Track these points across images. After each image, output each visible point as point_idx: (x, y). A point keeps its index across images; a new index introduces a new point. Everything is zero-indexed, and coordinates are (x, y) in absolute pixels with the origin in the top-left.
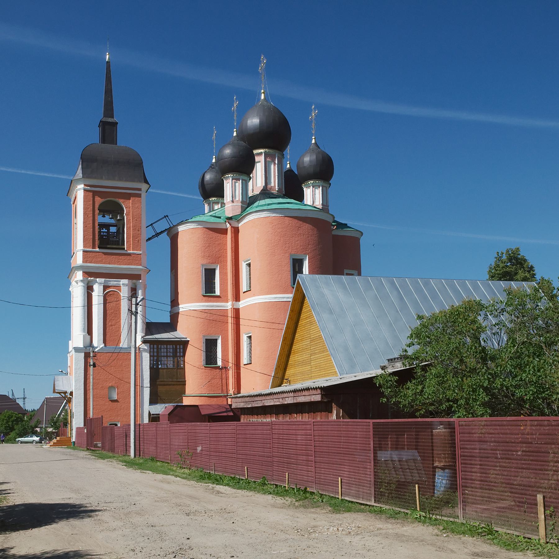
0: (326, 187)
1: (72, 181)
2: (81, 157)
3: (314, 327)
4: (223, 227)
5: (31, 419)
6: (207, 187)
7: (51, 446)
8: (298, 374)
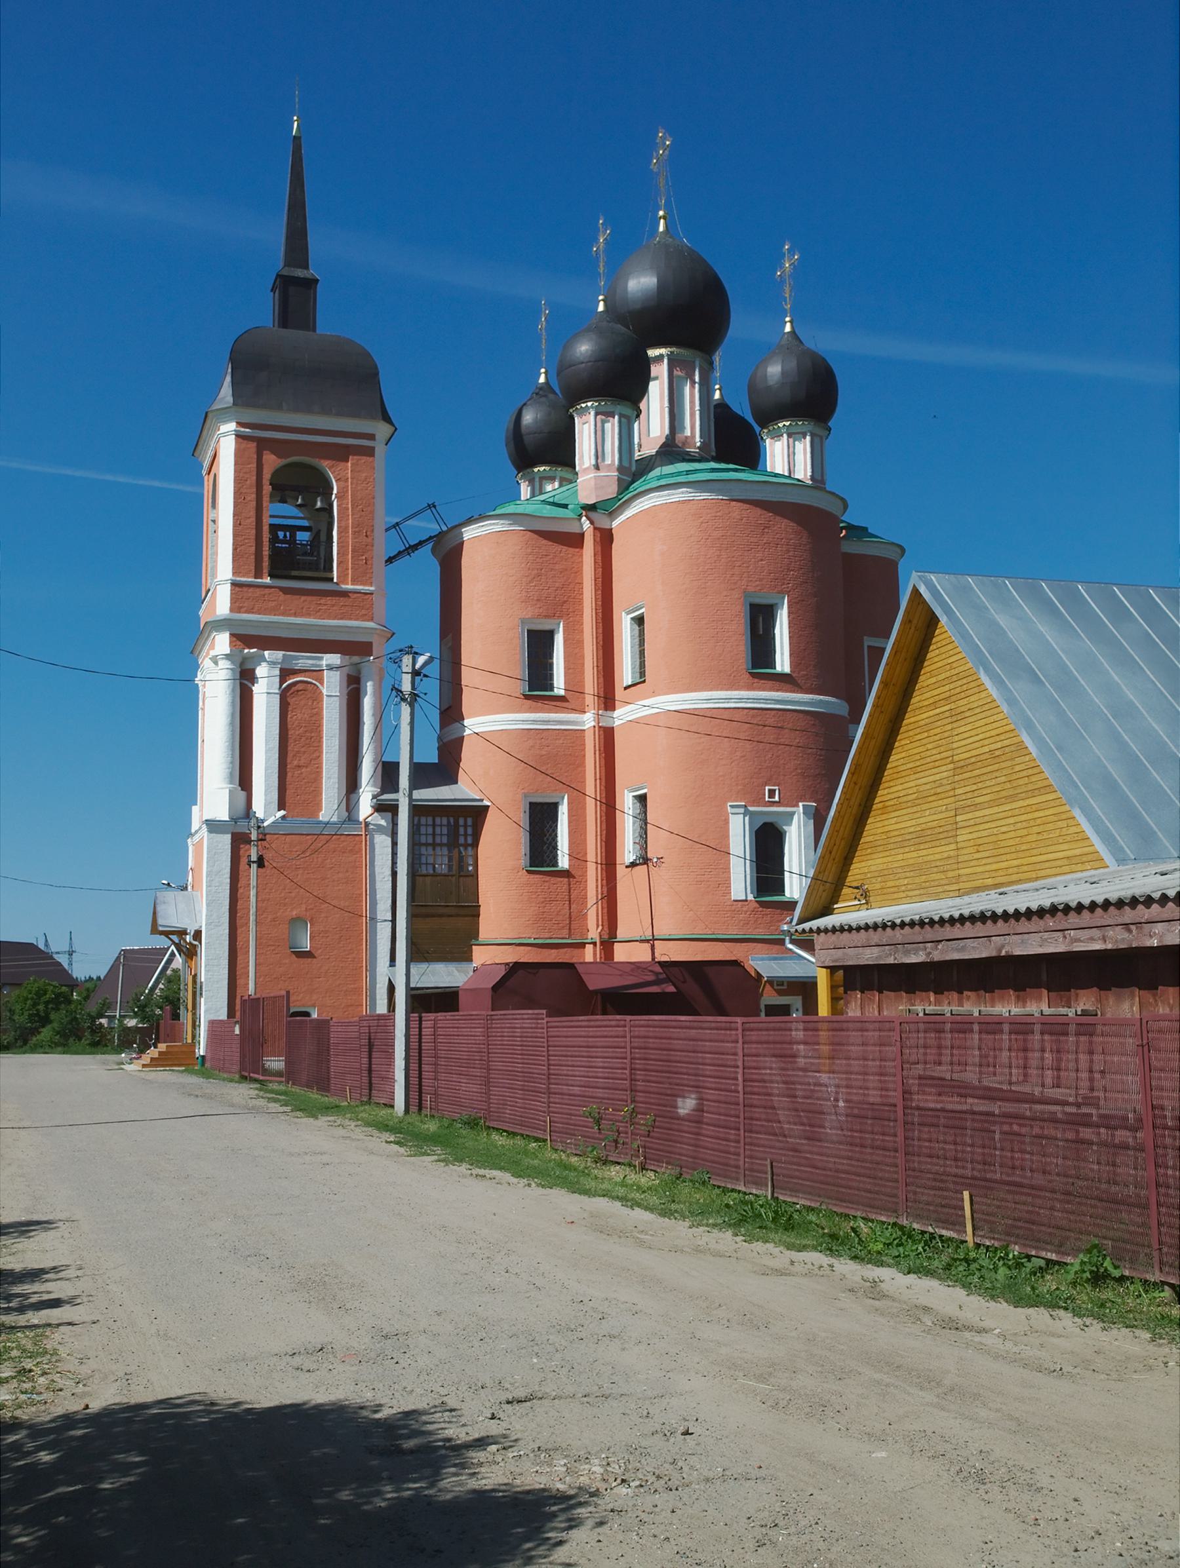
0: (821, 438)
1: (207, 413)
2: (230, 358)
3: (969, 727)
4: (573, 528)
5: (87, 998)
6: (527, 440)
7: (144, 1066)
8: (900, 870)
